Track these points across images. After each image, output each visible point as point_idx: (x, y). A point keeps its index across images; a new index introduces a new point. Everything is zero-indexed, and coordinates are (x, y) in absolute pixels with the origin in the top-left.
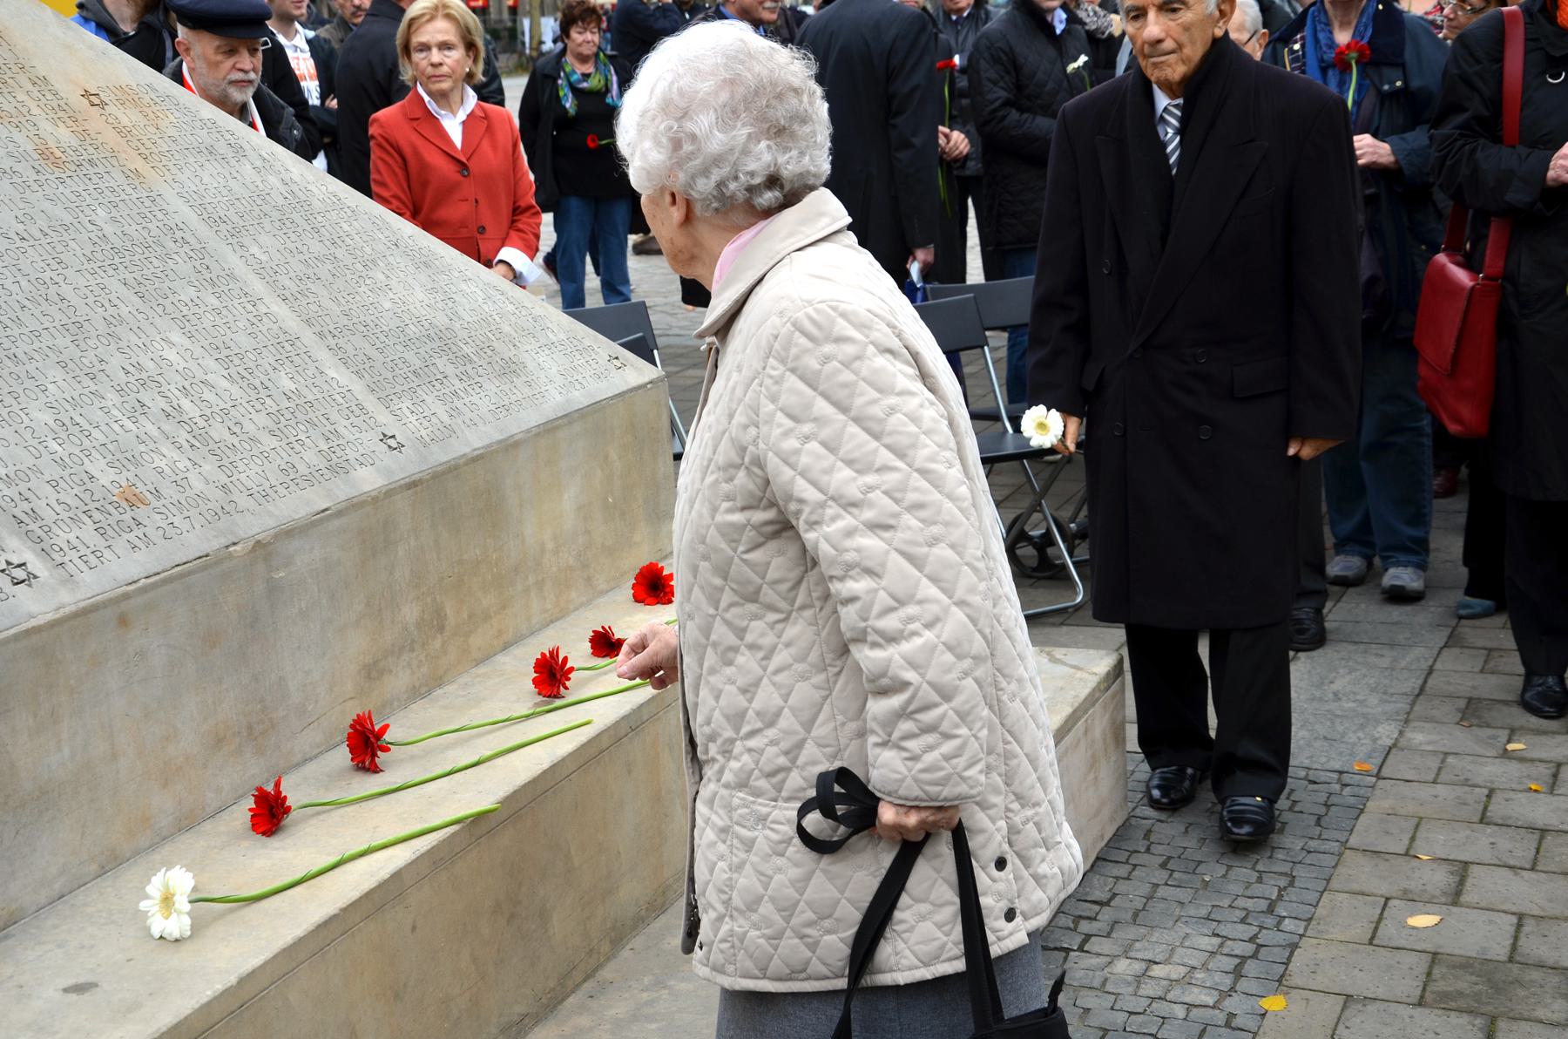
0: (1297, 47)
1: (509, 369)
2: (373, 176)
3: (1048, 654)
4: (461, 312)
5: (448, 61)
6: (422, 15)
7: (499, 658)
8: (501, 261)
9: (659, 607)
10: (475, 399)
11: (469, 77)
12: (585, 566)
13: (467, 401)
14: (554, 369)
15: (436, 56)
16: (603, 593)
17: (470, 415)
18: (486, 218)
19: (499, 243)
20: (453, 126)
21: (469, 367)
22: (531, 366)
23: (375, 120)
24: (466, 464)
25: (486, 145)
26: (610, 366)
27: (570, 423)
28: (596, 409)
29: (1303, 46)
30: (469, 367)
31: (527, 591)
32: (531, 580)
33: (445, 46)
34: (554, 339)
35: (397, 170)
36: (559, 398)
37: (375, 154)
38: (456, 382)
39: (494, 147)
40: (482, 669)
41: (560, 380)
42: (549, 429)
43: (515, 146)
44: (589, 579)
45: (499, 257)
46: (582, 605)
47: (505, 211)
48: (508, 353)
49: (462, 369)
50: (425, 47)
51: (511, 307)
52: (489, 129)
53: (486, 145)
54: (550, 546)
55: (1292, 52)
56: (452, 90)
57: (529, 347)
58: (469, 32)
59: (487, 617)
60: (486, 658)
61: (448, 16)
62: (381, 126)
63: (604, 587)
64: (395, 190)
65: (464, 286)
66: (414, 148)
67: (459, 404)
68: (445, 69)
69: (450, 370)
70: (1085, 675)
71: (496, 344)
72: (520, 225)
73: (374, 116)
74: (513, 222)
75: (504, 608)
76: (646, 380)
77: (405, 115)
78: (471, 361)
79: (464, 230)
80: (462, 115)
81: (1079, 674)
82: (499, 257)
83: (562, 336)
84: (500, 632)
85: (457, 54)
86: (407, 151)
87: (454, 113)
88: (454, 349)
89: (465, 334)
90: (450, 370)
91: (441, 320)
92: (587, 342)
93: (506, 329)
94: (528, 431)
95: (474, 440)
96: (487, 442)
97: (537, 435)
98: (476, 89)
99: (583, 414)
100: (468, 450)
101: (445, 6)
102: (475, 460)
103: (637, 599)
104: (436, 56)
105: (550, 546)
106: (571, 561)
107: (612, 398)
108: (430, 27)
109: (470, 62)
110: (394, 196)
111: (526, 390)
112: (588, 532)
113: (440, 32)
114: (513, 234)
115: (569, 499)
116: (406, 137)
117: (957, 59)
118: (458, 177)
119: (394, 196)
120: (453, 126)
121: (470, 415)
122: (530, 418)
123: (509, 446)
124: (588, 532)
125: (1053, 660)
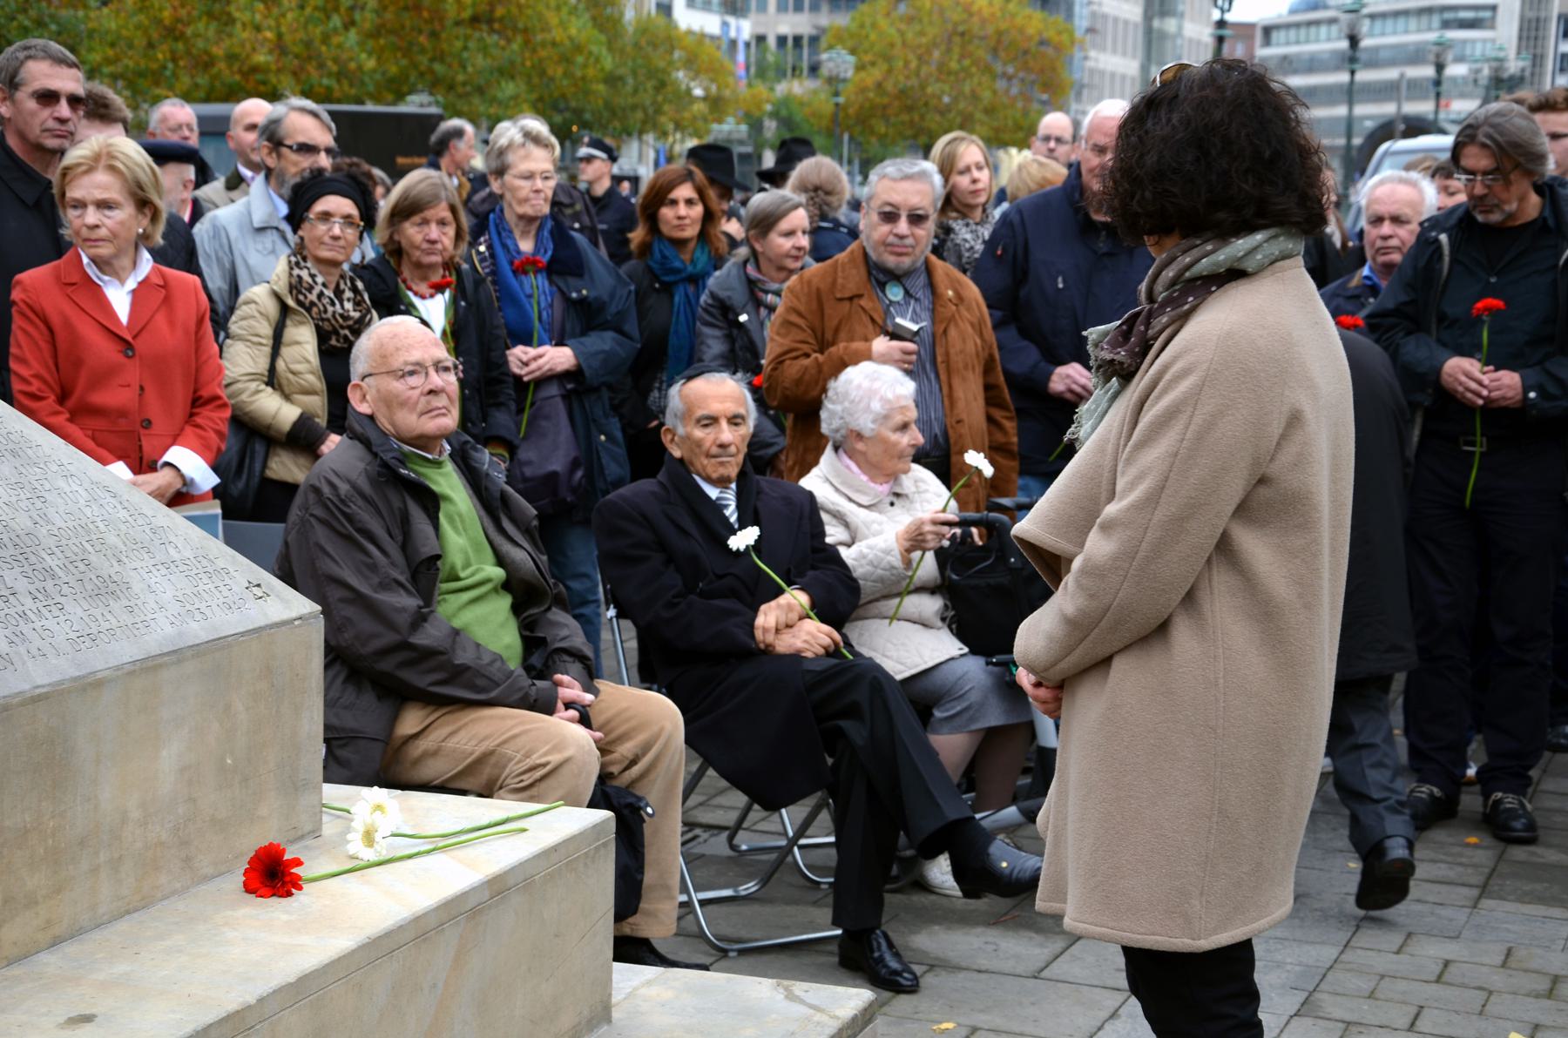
0: (482, 248)
1: (108, 590)
2: (13, 350)
3: (786, 989)
4: (51, 512)
5: (108, 222)
6: (79, 165)
7: (44, 957)
8: (168, 464)
9: (274, 900)
10: (48, 624)
11: (145, 238)
12: (185, 843)
13: (38, 625)
14: (169, 594)
15: (92, 216)
16: (207, 879)
17: (38, 642)
18: (154, 410)
19: (170, 440)
20: (119, 298)
21: (49, 584)
22: (137, 587)
23: (19, 282)
24: (23, 704)
25: (161, 320)
26: (248, 595)
27: (179, 661)
28: (219, 646)
29: (490, 247)
30: (49, 584)
31: (95, 870)
32: (103, 857)
33: (103, 205)
34: (176, 556)
35: (43, 344)
36: (169, 630)
37: (17, 322)
38: (29, 602)
39: (172, 323)
40: (16, 970)
41: (175, 608)
42: (150, 666)
43: (200, 322)
44: (188, 860)
45: (167, 457)
46: (174, 893)
47: (181, 398)
48: (108, 568)
49: (39, 585)
50: (81, 205)
51: (123, 514)
52: (167, 300)
53: (161, 320)
54: (135, 814)
55: (479, 253)
56: (116, 256)
57: (138, 564)
58: (140, 186)
59: (31, 902)
60: (24, 955)
61: (112, 169)
62: (25, 290)
63: (210, 871)
64: (37, 367)
65: (61, 483)
66: (68, 324)
67: (25, 628)
68: (103, 232)
69: (22, 585)
70: (825, 1018)
71: (93, 558)
72: (198, 420)
73: (19, 277)
74: (192, 415)
75: (59, 891)
76: (294, 614)
77: (58, 278)
78: (53, 577)
79: (122, 421)
80: (132, 284)
81: (818, 1017)
82: (167, 457)
83: (188, 554)
84: (49, 923)
85: (125, 213)
86: (56, 321)
87: (122, 282)
88: (33, 559)
89: (52, 542)
90: (22, 585)
91: (22, 522)
92: (221, 563)
93: (112, 539)
94: (117, 668)
95: (38, 674)
96: (56, 678)
97: (131, 673)
98: (152, 251)
99: (199, 651)
100: (27, 687)
101: (111, 156)
102: (36, 699)
103: (249, 889)
104: (92, 216)
105: (135, 814)
106: (164, 836)
107: (242, 634)
108: (86, 180)
109: (146, 222)
110: (36, 376)
111: (126, 618)
112: (192, 800)
113: (99, 187)
114: (189, 429)
115: (170, 757)
116: (56, 305)
117: (1493, 280)
118: (121, 359)
119: (36, 376)
120: (119, 298)
121: (38, 642)
122: (125, 651)
123: (90, 685)
124: (192, 800)
125: (791, 996)
